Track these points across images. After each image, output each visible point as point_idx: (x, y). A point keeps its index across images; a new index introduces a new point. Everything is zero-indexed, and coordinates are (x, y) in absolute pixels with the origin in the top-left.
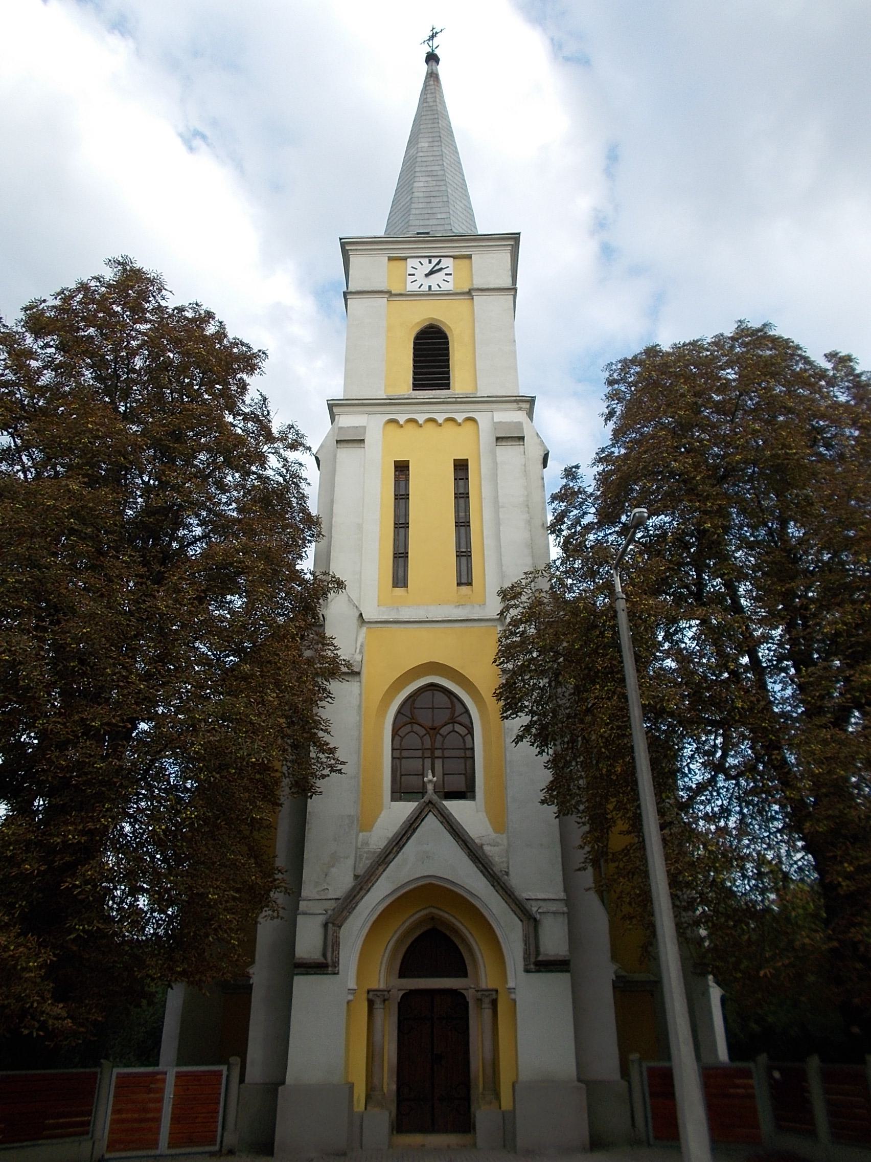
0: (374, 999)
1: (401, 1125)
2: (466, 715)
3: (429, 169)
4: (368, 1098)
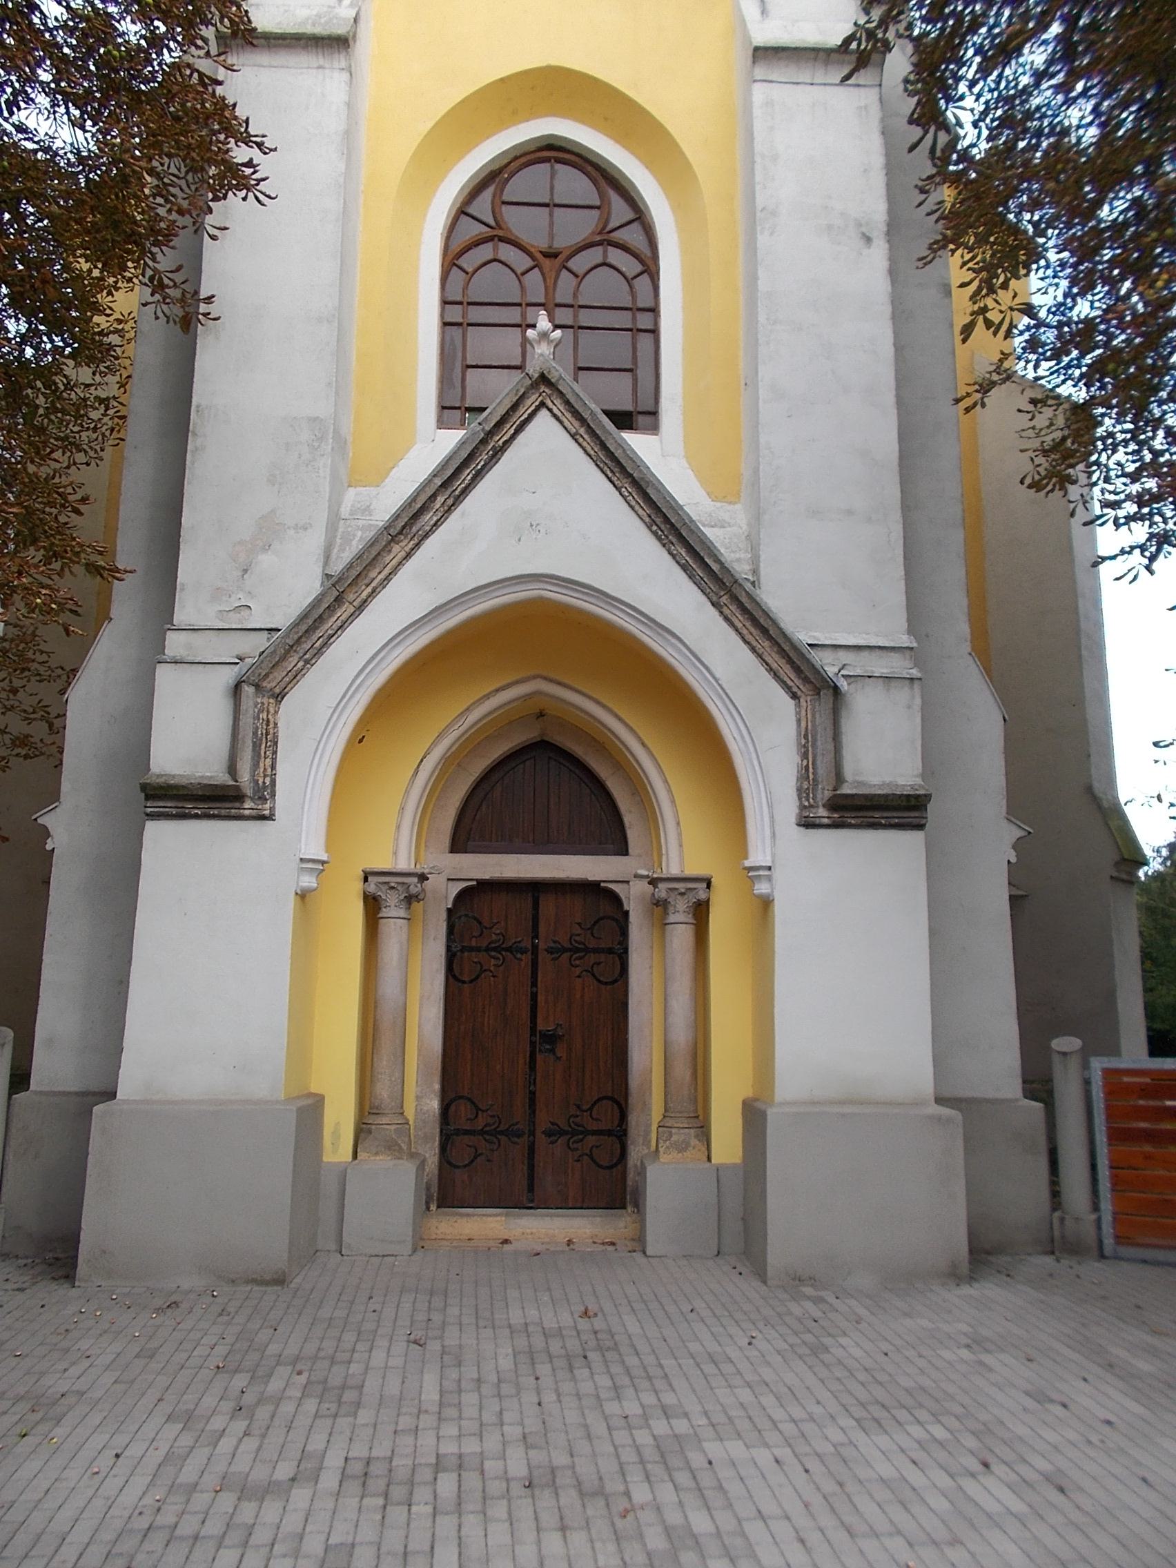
1: (448, 1191)
4: (362, 1131)
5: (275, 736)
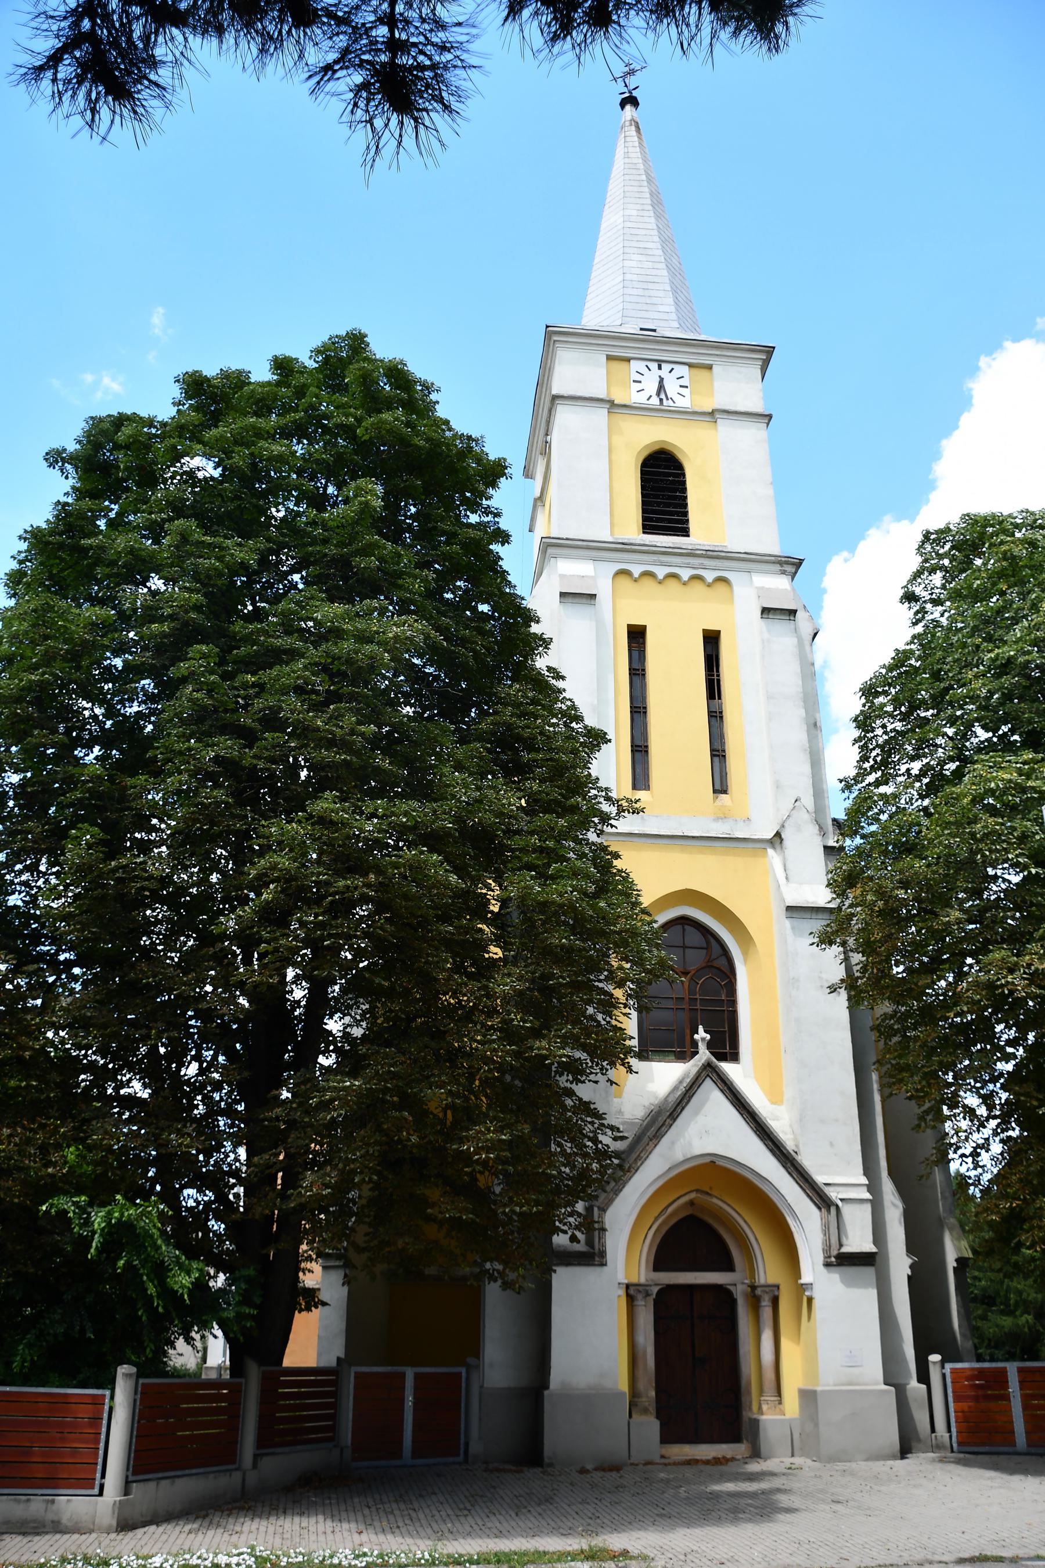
0: (632, 1293)
3: (641, 245)
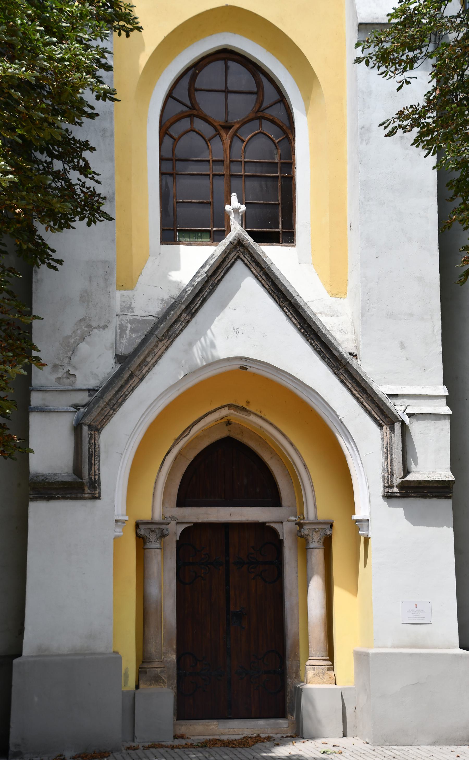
2: (280, 106)
4: (141, 671)
5: (99, 452)
